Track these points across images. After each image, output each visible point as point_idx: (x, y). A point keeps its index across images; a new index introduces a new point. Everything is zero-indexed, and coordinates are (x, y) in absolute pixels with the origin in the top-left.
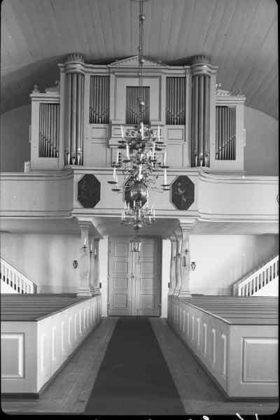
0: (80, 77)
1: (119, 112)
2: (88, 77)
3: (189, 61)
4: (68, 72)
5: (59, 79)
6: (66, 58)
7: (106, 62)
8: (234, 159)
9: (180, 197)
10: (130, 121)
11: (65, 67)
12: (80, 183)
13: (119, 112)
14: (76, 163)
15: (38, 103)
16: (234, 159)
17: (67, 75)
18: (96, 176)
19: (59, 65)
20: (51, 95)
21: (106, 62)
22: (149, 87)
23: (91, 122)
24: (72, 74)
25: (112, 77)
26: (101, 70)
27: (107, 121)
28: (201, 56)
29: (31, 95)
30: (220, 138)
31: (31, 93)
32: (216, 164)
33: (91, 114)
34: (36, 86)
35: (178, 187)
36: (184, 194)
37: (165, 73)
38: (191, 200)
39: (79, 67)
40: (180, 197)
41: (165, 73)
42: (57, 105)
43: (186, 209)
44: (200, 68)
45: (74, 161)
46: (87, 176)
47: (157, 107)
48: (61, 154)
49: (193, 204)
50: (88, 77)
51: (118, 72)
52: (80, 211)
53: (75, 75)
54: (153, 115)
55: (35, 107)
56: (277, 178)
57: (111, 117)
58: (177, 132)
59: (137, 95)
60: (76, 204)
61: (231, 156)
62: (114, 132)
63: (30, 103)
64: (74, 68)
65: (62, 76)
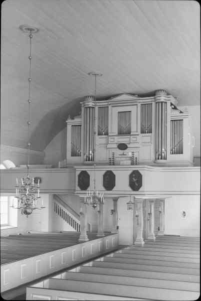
0: (163, 104)
1: (113, 128)
2: (97, 108)
3: (153, 94)
4: (157, 101)
5: (81, 110)
6: (84, 99)
7: (108, 98)
8: (182, 153)
9: (134, 183)
10: (120, 133)
11: (155, 98)
12: (79, 176)
13: (113, 128)
14: (161, 159)
15: (71, 126)
16: (182, 153)
17: (156, 103)
18: (88, 172)
19: (81, 103)
20: (77, 121)
21: (108, 98)
22: (130, 111)
23: (99, 135)
24: (159, 102)
25: (110, 107)
26: (103, 103)
27: (107, 134)
28: (159, 90)
29: (67, 121)
30: (173, 140)
31: (67, 120)
32: (171, 158)
33: (141, 128)
34: (69, 116)
35: (133, 177)
36: (137, 181)
37: (140, 102)
38: (140, 185)
39: (91, 104)
40: (134, 183)
41: (140, 102)
42: (81, 125)
43: (138, 191)
44: (160, 98)
45: (88, 159)
46: (108, 171)
47: (135, 125)
48: (82, 154)
49: (115, 187)
50: (97, 108)
51: (113, 104)
52: (79, 192)
53: (160, 104)
54: (133, 129)
55: (69, 127)
56: (200, 167)
57: (109, 131)
58: (147, 138)
59: (124, 116)
60: (78, 188)
61: (180, 152)
62: (110, 140)
63: (66, 126)
64: (159, 100)
65: (83, 109)
